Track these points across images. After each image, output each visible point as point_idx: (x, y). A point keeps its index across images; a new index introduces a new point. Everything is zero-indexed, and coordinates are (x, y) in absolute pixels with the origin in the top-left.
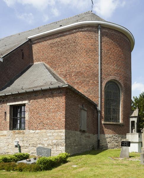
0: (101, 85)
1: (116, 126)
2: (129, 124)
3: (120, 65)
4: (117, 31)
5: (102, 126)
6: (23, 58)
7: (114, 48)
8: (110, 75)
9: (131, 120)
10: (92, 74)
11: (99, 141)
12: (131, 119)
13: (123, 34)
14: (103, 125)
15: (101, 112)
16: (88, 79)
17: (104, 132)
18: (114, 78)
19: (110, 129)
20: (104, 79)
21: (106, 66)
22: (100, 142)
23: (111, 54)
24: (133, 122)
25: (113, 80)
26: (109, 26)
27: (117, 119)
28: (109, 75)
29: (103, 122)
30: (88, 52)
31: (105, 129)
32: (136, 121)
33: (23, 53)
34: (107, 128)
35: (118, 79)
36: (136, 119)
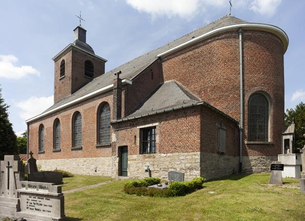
0: (243, 99)
6: (152, 78)
9: (284, 137)
11: (240, 164)
15: (243, 131)
17: (247, 153)
18: (260, 89)
23: (255, 61)
24: (287, 141)
28: (253, 86)
29: (246, 142)
33: (152, 73)
34: (252, 149)
35: (265, 89)
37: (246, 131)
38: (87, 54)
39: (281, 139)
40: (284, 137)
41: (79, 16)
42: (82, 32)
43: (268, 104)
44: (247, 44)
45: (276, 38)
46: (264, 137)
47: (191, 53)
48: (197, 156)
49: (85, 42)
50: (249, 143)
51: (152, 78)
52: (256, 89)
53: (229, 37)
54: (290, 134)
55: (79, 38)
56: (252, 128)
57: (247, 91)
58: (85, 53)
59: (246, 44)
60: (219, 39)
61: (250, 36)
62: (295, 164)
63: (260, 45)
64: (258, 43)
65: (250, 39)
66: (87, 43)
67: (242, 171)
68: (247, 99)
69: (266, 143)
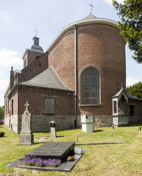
0: (77, 75)
1: (92, 108)
2: (112, 104)
3: (95, 53)
4: (92, 24)
5: (79, 108)
6: (40, 66)
7: (89, 40)
8: (86, 64)
9: (114, 100)
10: (71, 67)
11: (76, 121)
12: (31, 114)
13: (105, 24)
14: (80, 107)
15: (77, 97)
16: (68, 72)
17: (80, 113)
18: (89, 66)
19: (86, 110)
20: (80, 68)
21: (82, 57)
22: (77, 122)
23: (86, 47)
24: (115, 102)
25: (89, 67)
26: (85, 23)
27: (96, 101)
28: (84, 64)
29: (79, 105)
30: (69, 50)
31: (81, 111)
32: (117, 102)
33: (40, 63)
34: (84, 110)
35: (93, 65)
36: (117, 99)
37: (79, 97)
38: (37, 53)
39: (111, 102)
40: (114, 100)
41: (37, 33)
42: (36, 40)
43: (98, 75)
44: (81, 35)
45: (103, 26)
46: (97, 101)
47: (56, 47)
48: (17, 115)
49: (38, 46)
50: (83, 105)
51: (40, 66)
52: (88, 65)
53: (70, 33)
54: (116, 97)
55: (34, 44)
56: (86, 94)
57: (80, 68)
58: (36, 52)
59: (79, 36)
60: (66, 36)
61: (82, 29)
62: (85, 122)
63: (89, 34)
64: (87, 33)
65: (82, 31)
66: (39, 45)
67: (77, 127)
68: (79, 74)
69: (98, 105)
